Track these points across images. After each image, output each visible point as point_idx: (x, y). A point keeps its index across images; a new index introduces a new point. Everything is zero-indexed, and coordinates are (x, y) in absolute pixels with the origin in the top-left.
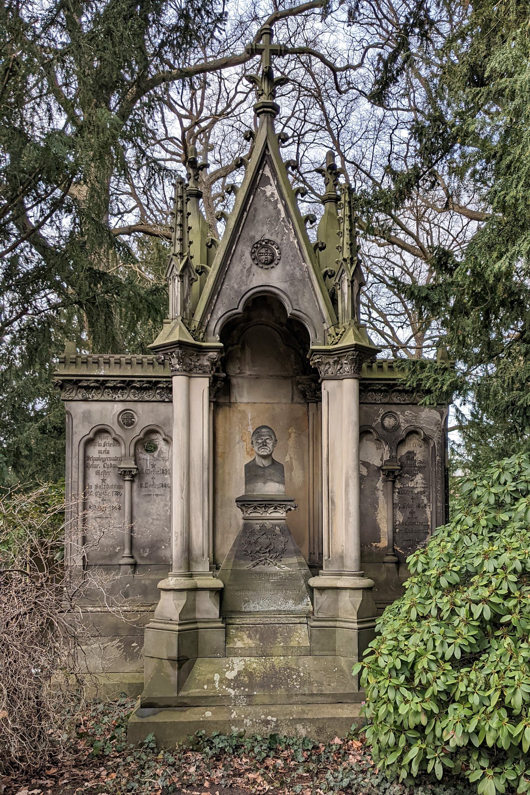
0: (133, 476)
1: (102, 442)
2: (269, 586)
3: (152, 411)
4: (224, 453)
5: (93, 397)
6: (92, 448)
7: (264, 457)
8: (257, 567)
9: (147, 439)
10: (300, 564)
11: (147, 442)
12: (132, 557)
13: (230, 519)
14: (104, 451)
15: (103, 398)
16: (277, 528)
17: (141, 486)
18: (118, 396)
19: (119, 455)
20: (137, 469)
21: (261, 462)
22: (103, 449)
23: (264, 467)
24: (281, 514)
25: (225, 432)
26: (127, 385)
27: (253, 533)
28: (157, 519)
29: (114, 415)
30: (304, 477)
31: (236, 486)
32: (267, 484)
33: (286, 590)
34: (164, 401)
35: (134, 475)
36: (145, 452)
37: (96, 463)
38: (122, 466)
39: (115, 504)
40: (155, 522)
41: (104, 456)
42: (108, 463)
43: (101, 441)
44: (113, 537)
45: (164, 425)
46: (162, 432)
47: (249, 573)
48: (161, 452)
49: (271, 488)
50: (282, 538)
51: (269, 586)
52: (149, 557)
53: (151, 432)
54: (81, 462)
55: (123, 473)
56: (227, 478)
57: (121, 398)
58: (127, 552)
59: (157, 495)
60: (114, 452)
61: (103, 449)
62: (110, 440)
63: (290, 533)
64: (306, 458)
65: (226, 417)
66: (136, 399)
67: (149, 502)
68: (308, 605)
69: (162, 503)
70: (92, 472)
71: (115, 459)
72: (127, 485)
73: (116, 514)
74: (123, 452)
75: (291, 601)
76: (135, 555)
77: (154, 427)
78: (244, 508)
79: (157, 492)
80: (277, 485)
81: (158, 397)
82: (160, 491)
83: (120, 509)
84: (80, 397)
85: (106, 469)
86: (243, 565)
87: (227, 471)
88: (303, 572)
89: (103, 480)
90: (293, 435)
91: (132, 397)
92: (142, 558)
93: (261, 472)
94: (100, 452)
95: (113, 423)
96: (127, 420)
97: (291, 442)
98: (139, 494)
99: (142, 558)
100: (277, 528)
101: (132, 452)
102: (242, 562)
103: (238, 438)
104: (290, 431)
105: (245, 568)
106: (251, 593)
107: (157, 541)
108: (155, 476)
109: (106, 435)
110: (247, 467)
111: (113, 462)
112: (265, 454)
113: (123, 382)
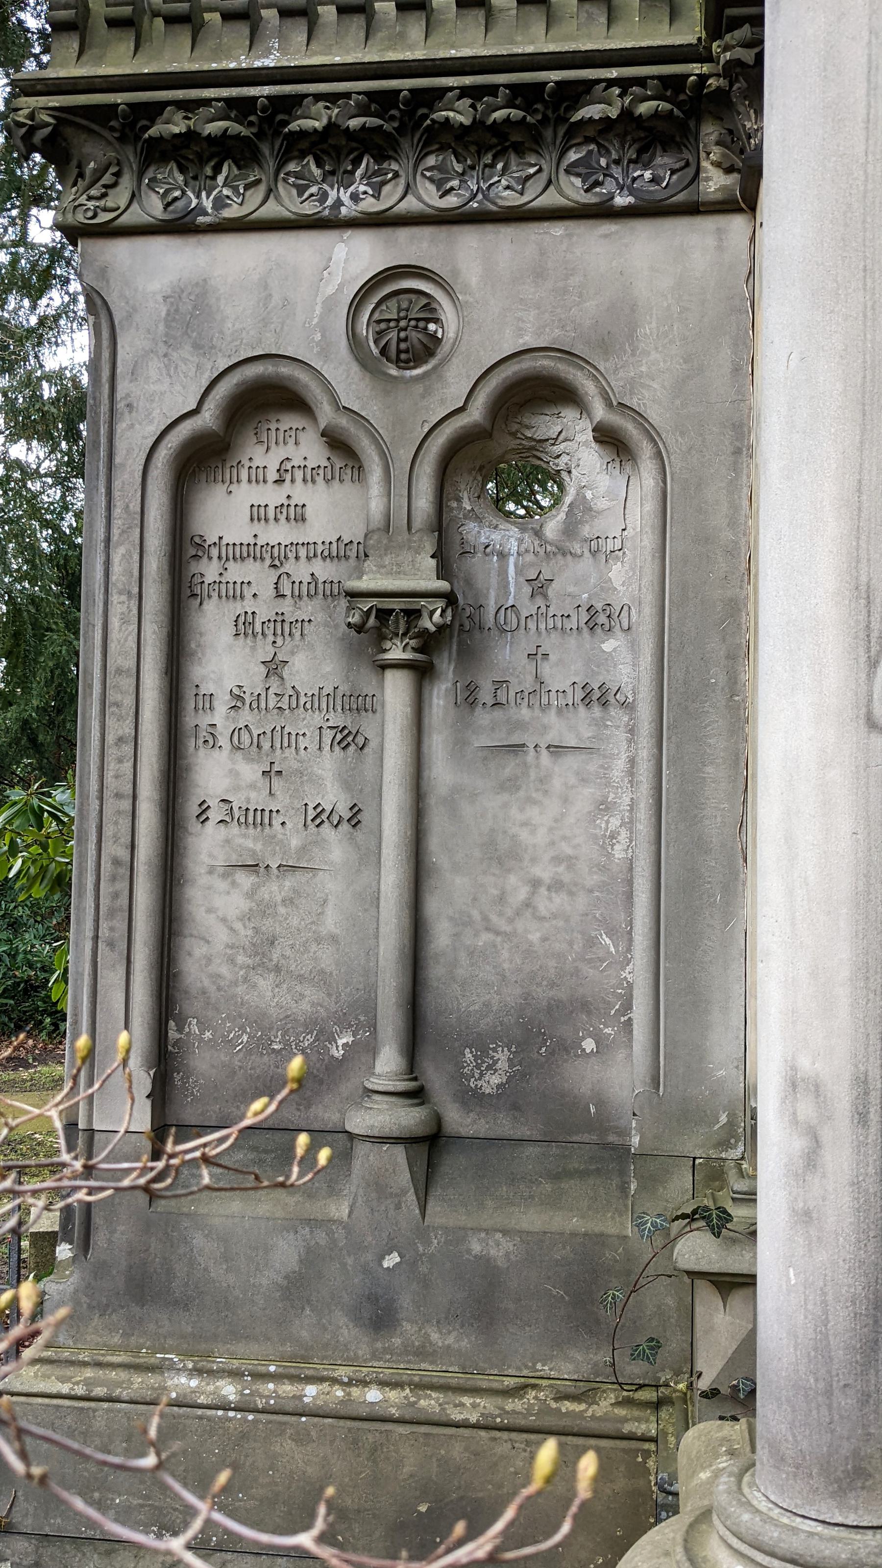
0: (429, 643)
1: (269, 460)
3: (539, 274)
5: (220, 203)
6: (220, 490)
9: (505, 443)
11: (499, 450)
12: (417, 1095)
14: (283, 509)
15: (271, 210)
17: (469, 698)
18: (352, 196)
19: (354, 532)
20: (450, 599)
22: (272, 496)
26: (396, 123)
28: (557, 886)
29: (330, 304)
34: (604, 212)
35: (428, 637)
36: (491, 517)
37: (236, 572)
38: (366, 583)
39: (333, 797)
40: (544, 904)
41: (278, 534)
42: (301, 571)
43: (261, 454)
44: (322, 978)
45: (605, 346)
46: (588, 387)
48: (582, 511)
52: (509, 1098)
53: (533, 390)
54: (155, 563)
55: (378, 622)
57: (369, 205)
58: (388, 1063)
59: (556, 750)
60: (332, 511)
61: (272, 496)
62: (310, 450)
66: (452, 201)
67: (510, 785)
69: (585, 797)
70: (213, 622)
71: (337, 552)
72: (396, 690)
73: (335, 846)
74: (376, 506)
76: (435, 1078)
77: (544, 363)
79: (557, 729)
81: (573, 191)
82: (579, 727)
83: (355, 819)
84: (153, 207)
85: (286, 606)
89: (274, 668)
91: (428, 196)
92: (471, 1099)
94: (258, 515)
95: (325, 351)
96: (400, 327)
98: (459, 744)
99: (471, 1099)
101: (424, 503)
107: (554, 1008)
108: (550, 643)
109: (290, 421)
111: (324, 570)
113: (381, 102)
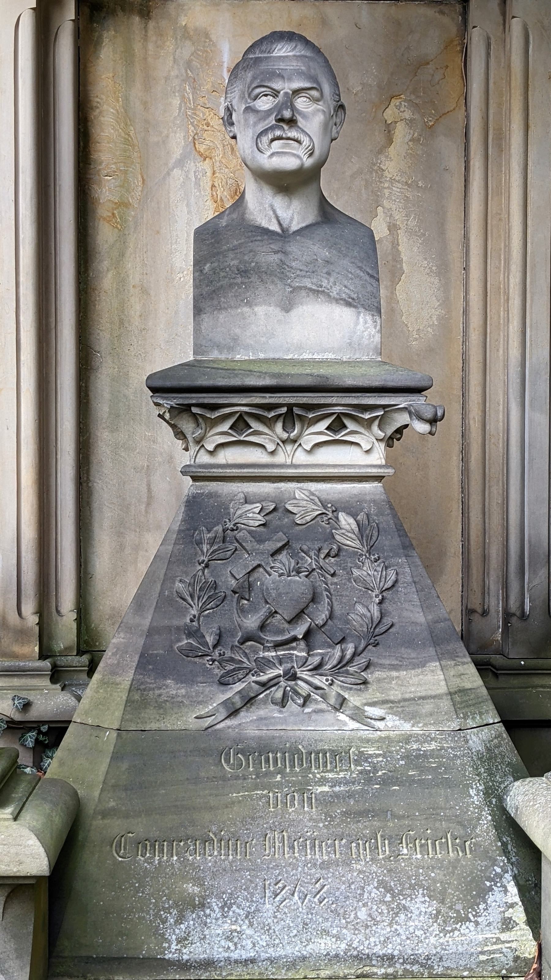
2: (305, 816)
4: (124, 204)
7: (284, 183)
8: (246, 717)
10: (460, 699)
13: (149, 470)
16: (346, 521)
21: (267, 209)
23: (284, 235)
24: (364, 452)
25: (126, 118)
27: (229, 541)
30: (446, 302)
31: (160, 325)
32: (295, 313)
33: (395, 840)
47: (208, 746)
49: (314, 331)
50: (368, 571)
51: (305, 816)
56: (135, 307)
63: (407, 546)
64: (454, 233)
65: (128, 57)
68: (507, 924)
75: (420, 906)
78: (187, 426)
80: (344, 314)
86: (177, 704)
87: (134, 277)
88: (477, 740)
90: (401, 133)
93: (268, 257)
97: (393, 163)
100: (346, 521)
102: (173, 688)
103: (177, 143)
104: (390, 114)
105: (189, 720)
106: (210, 858)
110: (210, 240)
112: (289, 163)
